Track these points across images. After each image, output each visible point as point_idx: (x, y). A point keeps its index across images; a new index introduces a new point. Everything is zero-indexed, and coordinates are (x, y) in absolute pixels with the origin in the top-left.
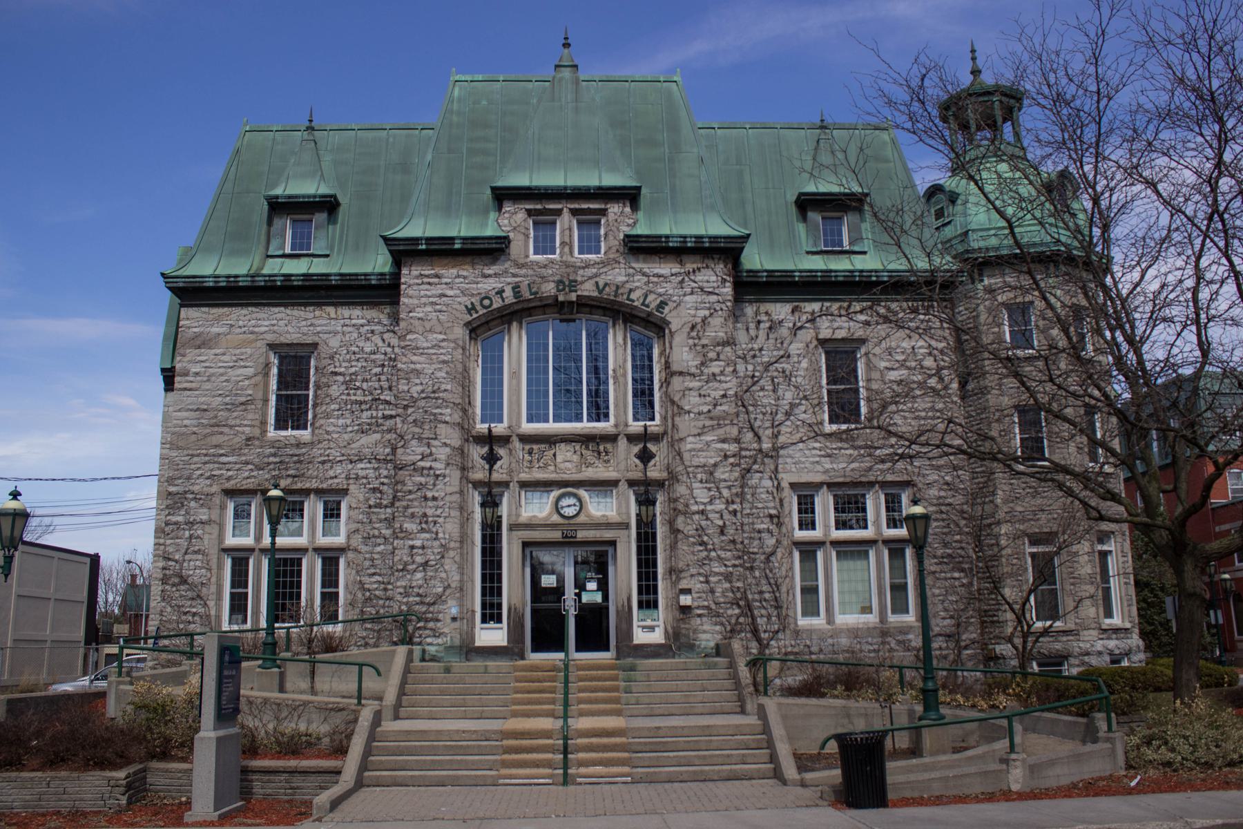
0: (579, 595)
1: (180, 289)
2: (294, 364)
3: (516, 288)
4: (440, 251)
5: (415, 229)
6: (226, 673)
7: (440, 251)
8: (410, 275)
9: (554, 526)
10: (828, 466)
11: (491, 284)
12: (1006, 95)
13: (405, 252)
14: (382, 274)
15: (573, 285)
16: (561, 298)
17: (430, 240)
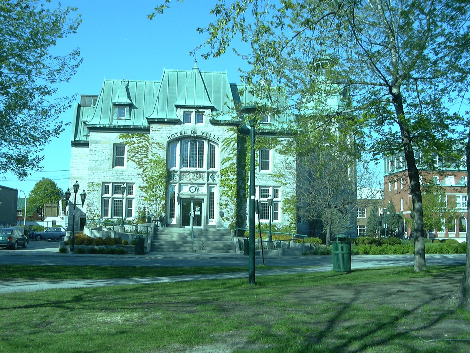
0: (194, 212)
1: (90, 127)
2: (118, 150)
3: (181, 133)
4: (161, 122)
5: (154, 116)
6: (121, 217)
7: (161, 122)
8: (153, 127)
9: (189, 194)
10: (20, 140)
11: (175, 130)
12: (10, 299)
13: (151, 121)
14: (145, 126)
15: (195, 132)
16: (192, 135)
17: (158, 119)
